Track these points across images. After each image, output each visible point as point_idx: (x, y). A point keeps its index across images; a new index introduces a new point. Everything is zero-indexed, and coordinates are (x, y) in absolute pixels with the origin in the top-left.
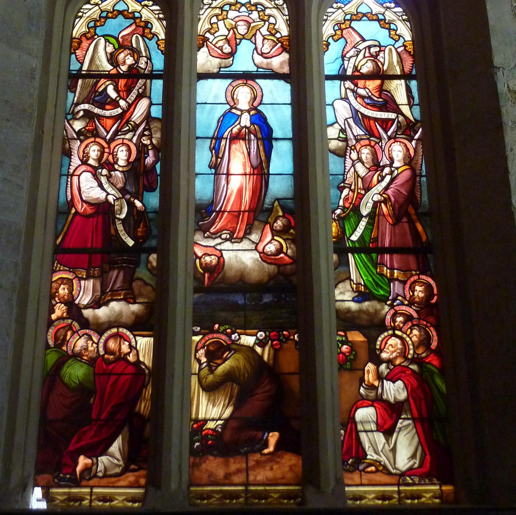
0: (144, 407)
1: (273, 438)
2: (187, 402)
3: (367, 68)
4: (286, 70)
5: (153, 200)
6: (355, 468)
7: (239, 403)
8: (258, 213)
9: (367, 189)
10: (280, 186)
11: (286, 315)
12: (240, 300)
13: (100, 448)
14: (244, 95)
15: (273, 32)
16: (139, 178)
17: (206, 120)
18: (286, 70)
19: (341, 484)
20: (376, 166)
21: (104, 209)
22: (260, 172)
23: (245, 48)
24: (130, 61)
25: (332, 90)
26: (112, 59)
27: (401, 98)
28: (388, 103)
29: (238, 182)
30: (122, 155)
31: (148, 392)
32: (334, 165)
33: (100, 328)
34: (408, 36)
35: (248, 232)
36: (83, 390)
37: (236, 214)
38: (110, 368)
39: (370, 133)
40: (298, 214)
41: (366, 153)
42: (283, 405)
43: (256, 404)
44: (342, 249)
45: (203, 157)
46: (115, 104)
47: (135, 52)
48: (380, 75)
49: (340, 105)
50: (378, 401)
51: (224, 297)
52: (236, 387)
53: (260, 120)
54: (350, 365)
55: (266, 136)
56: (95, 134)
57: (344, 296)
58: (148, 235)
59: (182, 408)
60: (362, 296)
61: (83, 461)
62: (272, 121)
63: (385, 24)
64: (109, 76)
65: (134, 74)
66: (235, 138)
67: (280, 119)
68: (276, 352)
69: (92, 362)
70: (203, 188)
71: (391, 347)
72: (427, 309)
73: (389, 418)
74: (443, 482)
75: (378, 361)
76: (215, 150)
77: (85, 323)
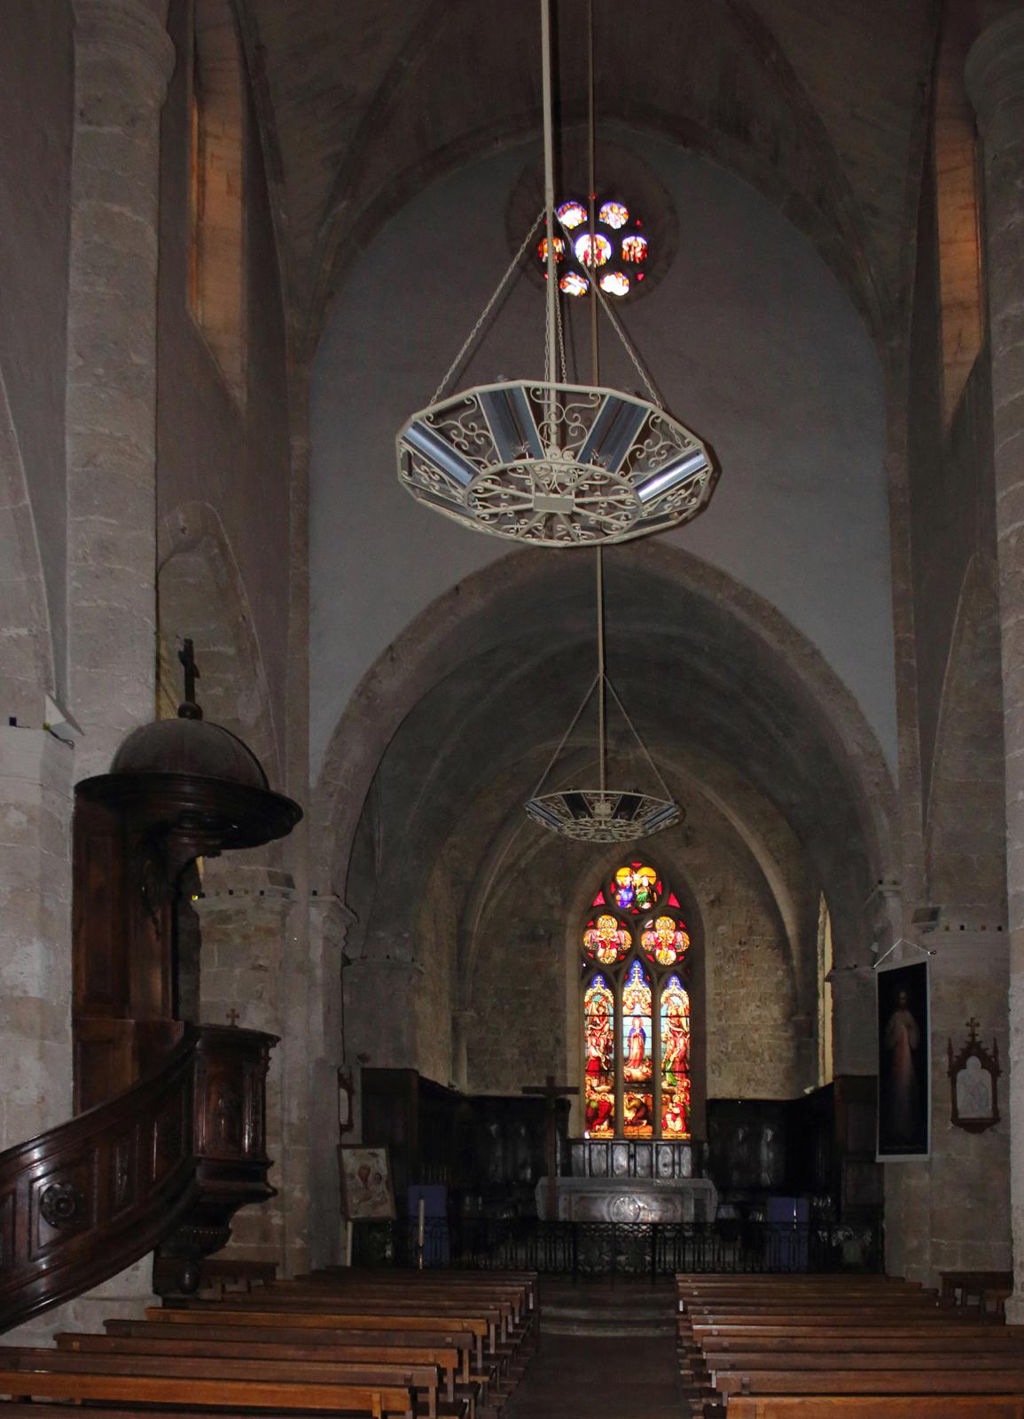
0: (612, 1113)
1: (645, 1122)
3: (674, 1013)
4: (650, 1014)
6: (665, 1130)
8: (641, 1061)
9: (673, 1053)
10: (648, 1052)
12: (636, 1085)
13: (601, 1124)
14: (637, 1022)
15: (646, 1000)
16: (607, 1049)
17: (626, 1031)
18: (650, 1014)
19: (661, 1133)
21: (598, 1059)
22: (642, 1048)
23: (637, 1006)
24: (603, 1010)
26: (598, 1010)
27: (684, 1024)
28: (680, 1026)
29: (635, 1051)
31: (613, 1110)
32: (663, 1045)
33: (599, 1093)
34: (688, 1003)
35: (639, 1065)
36: (596, 1110)
37: (635, 1061)
38: (602, 1103)
39: (674, 1035)
40: (654, 1061)
41: (673, 1042)
42: (648, 1114)
43: (641, 1113)
44: (664, 1071)
46: (599, 1025)
47: (604, 1007)
48: (678, 1016)
49: (666, 1026)
51: (633, 1085)
52: (637, 1109)
53: (642, 1031)
54: (666, 1104)
56: (594, 1035)
57: (664, 1085)
58: (611, 1067)
59: (741, 1336)
60: (670, 1085)
61: (597, 1127)
62: (645, 1031)
64: (597, 1016)
65: (604, 1015)
66: (634, 1037)
67: (648, 1032)
68: (646, 1100)
69: (598, 1102)
70: (626, 1053)
71: (676, 1099)
72: (687, 1089)
73: (675, 1116)
74: (688, 1133)
75: (672, 1102)
76: (629, 1041)
77: (595, 1091)
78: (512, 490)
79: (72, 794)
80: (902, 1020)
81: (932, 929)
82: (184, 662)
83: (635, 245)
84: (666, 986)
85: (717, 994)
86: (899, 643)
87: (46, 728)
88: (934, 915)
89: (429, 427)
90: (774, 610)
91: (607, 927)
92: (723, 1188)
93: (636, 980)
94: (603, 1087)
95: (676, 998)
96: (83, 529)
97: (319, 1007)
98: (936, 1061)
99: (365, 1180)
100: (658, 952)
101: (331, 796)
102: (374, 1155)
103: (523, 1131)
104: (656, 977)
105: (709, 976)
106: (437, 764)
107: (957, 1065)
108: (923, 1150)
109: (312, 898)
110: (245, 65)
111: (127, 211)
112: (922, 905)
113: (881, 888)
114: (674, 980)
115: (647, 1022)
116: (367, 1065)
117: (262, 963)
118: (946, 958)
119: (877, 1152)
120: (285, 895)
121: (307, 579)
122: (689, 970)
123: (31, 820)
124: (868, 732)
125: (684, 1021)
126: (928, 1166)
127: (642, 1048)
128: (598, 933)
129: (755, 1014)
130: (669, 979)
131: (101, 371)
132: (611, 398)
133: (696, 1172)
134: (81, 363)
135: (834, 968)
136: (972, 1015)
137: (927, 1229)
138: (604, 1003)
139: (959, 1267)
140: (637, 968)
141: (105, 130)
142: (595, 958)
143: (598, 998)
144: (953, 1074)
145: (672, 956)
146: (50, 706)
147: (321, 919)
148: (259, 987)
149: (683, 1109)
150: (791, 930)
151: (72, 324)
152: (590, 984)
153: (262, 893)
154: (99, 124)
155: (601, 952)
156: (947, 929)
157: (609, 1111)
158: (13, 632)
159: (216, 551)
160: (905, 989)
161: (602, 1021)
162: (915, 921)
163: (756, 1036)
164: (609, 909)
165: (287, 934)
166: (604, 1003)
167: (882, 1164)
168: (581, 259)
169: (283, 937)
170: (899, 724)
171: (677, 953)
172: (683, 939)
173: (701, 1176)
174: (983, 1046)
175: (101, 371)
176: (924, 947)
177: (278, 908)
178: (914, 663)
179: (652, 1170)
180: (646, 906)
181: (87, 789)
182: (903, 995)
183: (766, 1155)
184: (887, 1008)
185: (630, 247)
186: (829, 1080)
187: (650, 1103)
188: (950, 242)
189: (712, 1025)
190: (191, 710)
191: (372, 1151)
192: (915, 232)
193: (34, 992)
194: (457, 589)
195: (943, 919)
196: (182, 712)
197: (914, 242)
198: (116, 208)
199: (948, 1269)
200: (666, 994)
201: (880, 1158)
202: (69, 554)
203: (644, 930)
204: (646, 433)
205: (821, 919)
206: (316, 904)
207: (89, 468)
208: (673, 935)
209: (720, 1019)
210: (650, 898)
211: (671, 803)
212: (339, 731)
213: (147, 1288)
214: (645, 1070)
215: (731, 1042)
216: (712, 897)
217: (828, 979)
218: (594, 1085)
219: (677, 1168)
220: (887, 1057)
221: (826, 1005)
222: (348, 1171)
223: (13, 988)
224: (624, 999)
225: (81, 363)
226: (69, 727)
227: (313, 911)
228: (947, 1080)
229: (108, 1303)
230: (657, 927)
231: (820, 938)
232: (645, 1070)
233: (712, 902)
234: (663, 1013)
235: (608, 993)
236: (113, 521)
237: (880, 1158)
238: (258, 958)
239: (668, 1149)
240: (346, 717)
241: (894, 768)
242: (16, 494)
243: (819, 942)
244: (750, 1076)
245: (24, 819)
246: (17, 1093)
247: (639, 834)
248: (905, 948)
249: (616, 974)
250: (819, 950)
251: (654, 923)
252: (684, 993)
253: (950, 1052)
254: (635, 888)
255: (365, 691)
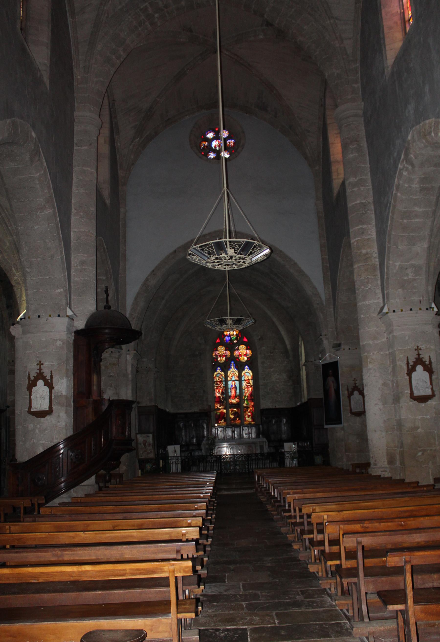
0: (225, 416)
2: (229, 416)
3: (247, 379)
5: (225, 396)
7: (234, 416)
8: (235, 397)
11: (261, 429)
14: (233, 383)
17: (230, 386)
20: (248, 391)
21: (219, 397)
22: (236, 392)
23: (233, 377)
25: (243, 382)
28: (249, 383)
29: (233, 393)
30: (221, 391)
32: (243, 391)
36: (219, 415)
38: (222, 413)
40: (240, 396)
42: (239, 415)
44: (244, 400)
45: (229, 391)
48: (249, 380)
50: (248, 415)
51: (233, 405)
53: (235, 386)
54: (245, 412)
55: (236, 387)
57: (245, 405)
60: (246, 405)
63: (249, 373)
65: (221, 381)
67: (238, 386)
70: (230, 394)
72: (253, 406)
73: (249, 416)
78: (218, 260)
79: (73, 334)
80: (331, 380)
81: (339, 349)
82: (106, 293)
83: (231, 142)
84: (244, 369)
85: (263, 371)
86: (323, 259)
87: (67, 316)
88: (339, 345)
89: (199, 249)
90: (281, 251)
91: (221, 350)
92: (269, 441)
93: (233, 368)
94: (222, 407)
95: (248, 373)
96: (76, 258)
97: (130, 387)
98: (343, 393)
99: (145, 445)
100: (240, 357)
101: (134, 319)
102: (148, 436)
103: (192, 425)
104: (240, 367)
105: (260, 364)
106: (164, 301)
107: (350, 394)
108: (340, 423)
109: (128, 352)
110: (109, 106)
111: (89, 169)
112: (335, 342)
113: (321, 337)
114: (246, 367)
115: (237, 383)
116: (139, 405)
117: (111, 375)
118: (344, 359)
119: (277, 611)
120: (119, 352)
121: (125, 251)
122: (251, 363)
123: (63, 343)
124: (315, 288)
125: (251, 381)
126: (343, 429)
127: (236, 392)
128: (218, 352)
129: (278, 378)
130: (245, 367)
131: (82, 214)
132: (246, 241)
133: (258, 436)
134: (76, 211)
135: (306, 361)
136: (354, 377)
137: (28, 159)
138: (221, 377)
139: (356, 462)
140: (233, 364)
141: (83, 148)
142: (218, 361)
143: (219, 375)
144: (349, 397)
145: (246, 358)
146: (68, 310)
147: (130, 359)
148: (111, 383)
149: (252, 414)
150: (289, 347)
151: (73, 201)
152: (216, 371)
153: (112, 352)
154: (81, 146)
155: (219, 359)
156: (344, 349)
157: (224, 416)
158: (59, 291)
159: (102, 250)
160: (331, 369)
161: (220, 383)
162: (333, 347)
163: (278, 385)
164: (222, 344)
165: (120, 365)
166: (221, 377)
167: (327, 429)
168: (214, 148)
169: (118, 366)
170: (324, 284)
171: (247, 358)
172: (249, 352)
173: (259, 437)
174: (359, 387)
175: (82, 214)
176: (337, 356)
177: (117, 356)
178: (328, 265)
179: (240, 435)
180: (235, 341)
181: (78, 333)
182: (330, 371)
183: (284, 428)
184: (325, 376)
185: (229, 142)
186: (306, 400)
187: (239, 412)
188: (333, 143)
189: (261, 382)
190: (108, 307)
191: (147, 435)
192: (322, 137)
193: (64, 393)
194: (175, 251)
195: (342, 346)
196: (105, 308)
197: (321, 140)
198: (86, 169)
199: (353, 463)
200: (244, 372)
201: (326, 427)
202: (72, 265)
203: (235, 350)
204: (255, 247)
205: (300, 343)
206: (129, 354)
207: (79, 241)
208: (245, 351)
209: (264, 380)
210: (236, 339)
211: (252, 319)
212: (136, 299)
213: (94, 482)
214: (237, 400)
215: (268, 388)
216: (259, 337)
217: (304, 365)
218: (218, 406)
219: (250, 435)
220: (326, 392)
221: (303, 373)
222: (139, 442)
223: (58, 393)
224: (228, 375)
225: (76, 211)
226: (74, 316)
227: (128, 356)
228: (347, 399)
229: (84, 487)
230: (240, 348)
231: (300, 349)
232: (237, 400)
233: (260, 339)
234: (243, 379)
235: (222, 373)
236: (85, 255)
237: (326, 427)
238: (110, 373)
239: (247, 428)
240: (138, 294)
241: (323, 297)
242: (61, 252)
243: (300, 351)
244: (278, 399)
245: (61, 343)
246: (59, 424)
247: (242, 328)
248: (330, 356)
249: (225, 366)
250: (300, 354)
251: (238, 348)
252: (250, 372)
253: (348, 390)
254: (231, 335)
255: (145, 284)
